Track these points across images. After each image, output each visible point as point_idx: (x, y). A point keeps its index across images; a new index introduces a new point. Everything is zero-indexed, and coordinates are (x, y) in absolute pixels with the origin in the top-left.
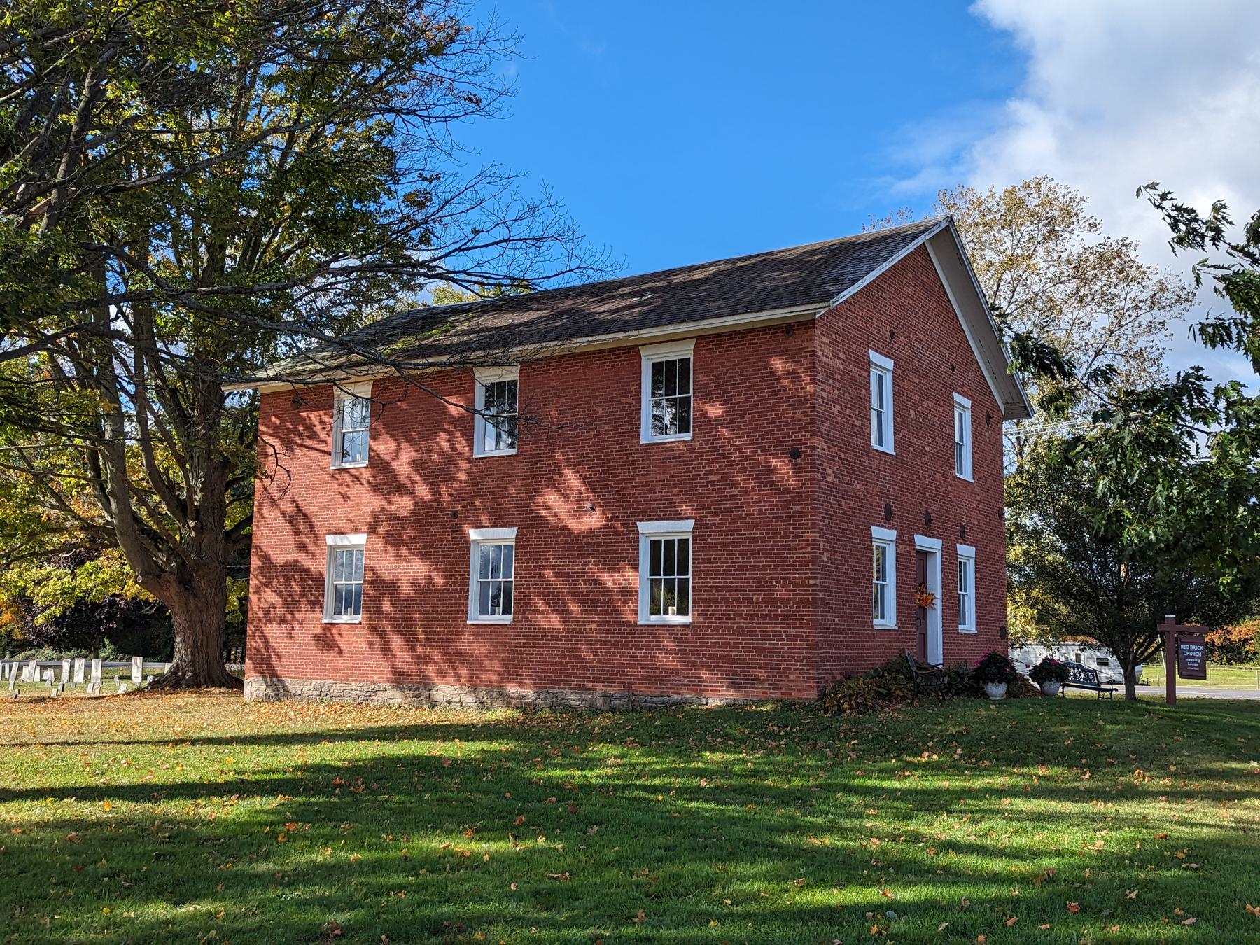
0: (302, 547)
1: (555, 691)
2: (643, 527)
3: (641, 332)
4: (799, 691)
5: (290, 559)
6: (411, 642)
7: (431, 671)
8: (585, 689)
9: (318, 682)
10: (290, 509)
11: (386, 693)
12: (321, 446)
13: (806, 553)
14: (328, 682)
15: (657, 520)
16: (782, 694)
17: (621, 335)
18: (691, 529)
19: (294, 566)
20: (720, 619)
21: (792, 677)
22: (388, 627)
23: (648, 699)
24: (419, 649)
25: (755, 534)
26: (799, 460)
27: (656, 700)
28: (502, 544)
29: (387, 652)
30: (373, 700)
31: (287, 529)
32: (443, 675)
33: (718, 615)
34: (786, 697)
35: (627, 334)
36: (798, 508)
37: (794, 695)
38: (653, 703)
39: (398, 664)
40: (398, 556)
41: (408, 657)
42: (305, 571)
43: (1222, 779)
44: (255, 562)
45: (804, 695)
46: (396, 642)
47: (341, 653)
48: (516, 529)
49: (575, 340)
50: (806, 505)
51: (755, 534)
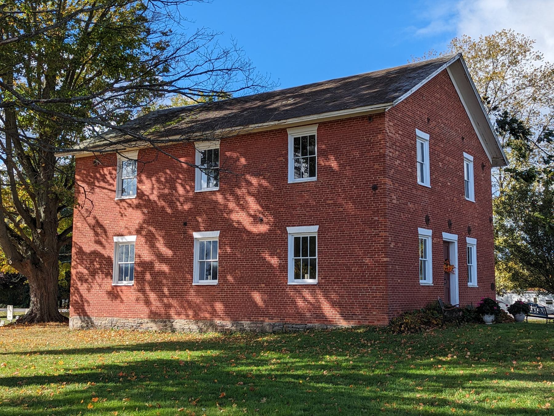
2: (290, 230)
4: (378, 320)
6: (161, 296)
7: (172, 312)
9: (110, 318)
11: (148, 324)
12: (109, 187)
13: (382, 243)
14: (115, 318)
15: (298, 226)
16: (369, 322)
19: (95, 253)
20: (334, 281)
21: (374, 313)
22: (147, 288)
23: (294, 326)
25: (353, 233)
26: (377, 191)
27: (298, 327)
29: (147, 302)
30: (141, 328)
31: (92, 233)
32: (179, 314)
33: (333, 279)
34: (371, 324)
36: (376, 218)
37: (376, 323)
38: (297, 328)
39: (153, 308)
40: (137, 300)
42: (101, 256)
45: (381, 323)
46: (152, 296)
47: (122, 301)
48: (219, 232)
50: (381, 216)
51: (353, 233)
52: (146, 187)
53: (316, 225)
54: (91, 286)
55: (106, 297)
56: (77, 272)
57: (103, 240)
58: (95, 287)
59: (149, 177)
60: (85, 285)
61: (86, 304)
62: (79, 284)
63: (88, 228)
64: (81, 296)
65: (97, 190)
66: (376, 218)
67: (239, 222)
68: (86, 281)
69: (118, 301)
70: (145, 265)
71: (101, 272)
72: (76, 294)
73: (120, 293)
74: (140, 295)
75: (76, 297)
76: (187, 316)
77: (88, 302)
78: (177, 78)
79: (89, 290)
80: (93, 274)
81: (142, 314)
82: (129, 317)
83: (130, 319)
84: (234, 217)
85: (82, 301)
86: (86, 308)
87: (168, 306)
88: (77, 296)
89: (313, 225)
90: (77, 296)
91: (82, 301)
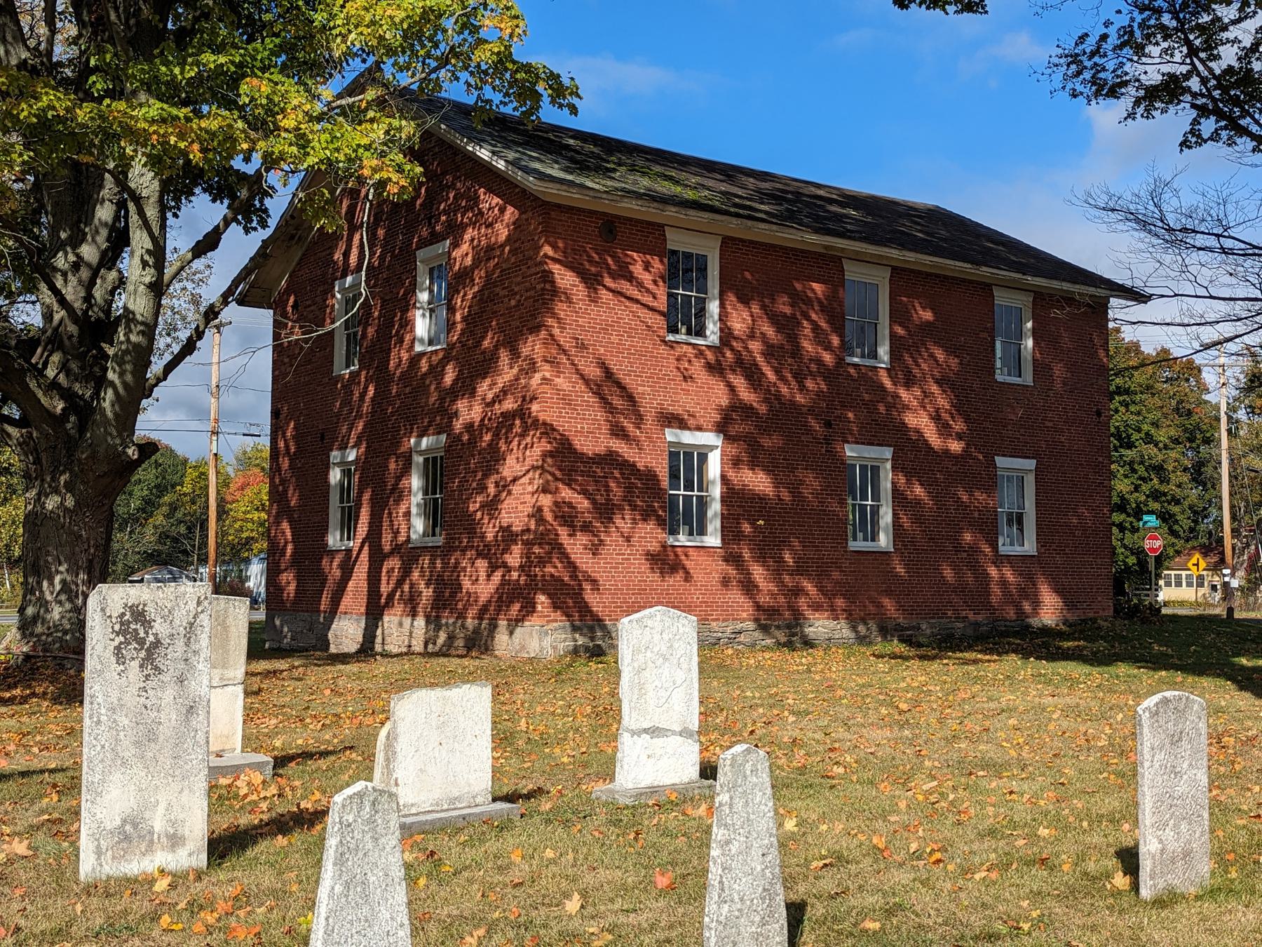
0: (618, 432)
1: (934, 621)
2: (1001, 461)
3: (1035, 279)
5: (601, 449)
6: (777, 571)
7: (802, 602)
8: (959, 618)
10: (594, 372)
12: (648, 299)
15: (1010, 456)
17: (1020, 276)
18: (1033, 467)
19: (610, 459)
21: (1099, 599)
24: (787, 578)
28: (869, 464)
29: (749, 587)
31: (589, 398)
32: (817, 607)
35: (1024, 277)
36: (1101, 459)
39: (764, 599)
40: (725, 582)
41: (772, 586)
42: (628, 468)
43: (572, 182)
44: (319, 827)
46: (758, 573)
47: (688, 577)
49: (984, 269)
52: (738, 325)
53: (1033, 458)
54: (601, 541)
55: (645, 567)
56: (556, 504)
57: (630, 427)
58: (612, 540)
59: (745, 300)
60: (583, 539)
61: (587, 587)
62: (563, 532)
63: (581, 386)
64: (572, 567)
65: (604, 295)
66: (1101, 459)
67: (918, 431)
68: (586, 528)
69: (680, 576)
70: (747, 502)
71: (630, 505)
72: (554, 560)
73: (683, 558)
74: (732, 572)
75: (556, 567)
76: (833, 609)
77: (594, 582)
78: (1216, 337)
79: (595, 549)
80: (606, 512)
81: (743, 611)
82: (714, 620)
83: (714, 624)
84: (911, 420)
85: (574, 576)
86: (590, 597)
87: (798, 591)
88: (559, 565)
89: (1028, 458)
90: (559, 565)
91: (574, 576)
